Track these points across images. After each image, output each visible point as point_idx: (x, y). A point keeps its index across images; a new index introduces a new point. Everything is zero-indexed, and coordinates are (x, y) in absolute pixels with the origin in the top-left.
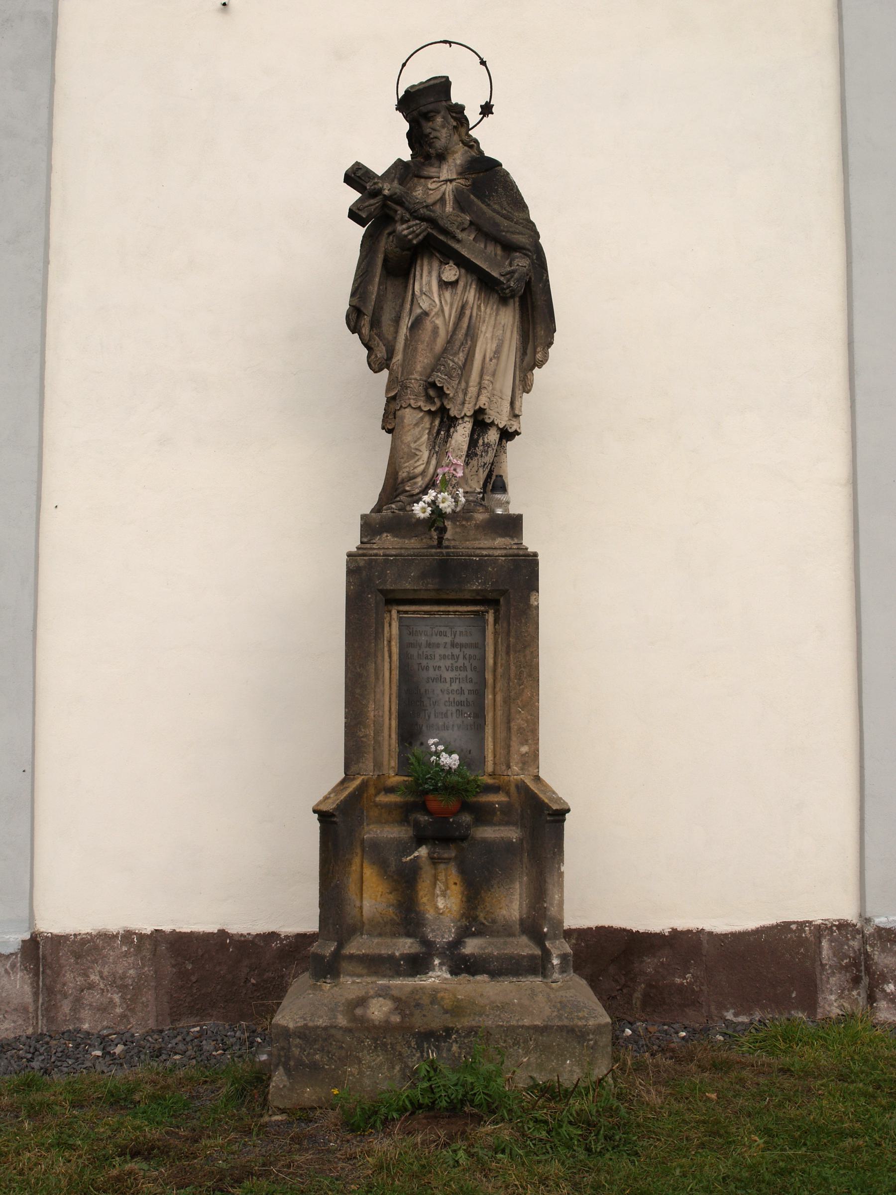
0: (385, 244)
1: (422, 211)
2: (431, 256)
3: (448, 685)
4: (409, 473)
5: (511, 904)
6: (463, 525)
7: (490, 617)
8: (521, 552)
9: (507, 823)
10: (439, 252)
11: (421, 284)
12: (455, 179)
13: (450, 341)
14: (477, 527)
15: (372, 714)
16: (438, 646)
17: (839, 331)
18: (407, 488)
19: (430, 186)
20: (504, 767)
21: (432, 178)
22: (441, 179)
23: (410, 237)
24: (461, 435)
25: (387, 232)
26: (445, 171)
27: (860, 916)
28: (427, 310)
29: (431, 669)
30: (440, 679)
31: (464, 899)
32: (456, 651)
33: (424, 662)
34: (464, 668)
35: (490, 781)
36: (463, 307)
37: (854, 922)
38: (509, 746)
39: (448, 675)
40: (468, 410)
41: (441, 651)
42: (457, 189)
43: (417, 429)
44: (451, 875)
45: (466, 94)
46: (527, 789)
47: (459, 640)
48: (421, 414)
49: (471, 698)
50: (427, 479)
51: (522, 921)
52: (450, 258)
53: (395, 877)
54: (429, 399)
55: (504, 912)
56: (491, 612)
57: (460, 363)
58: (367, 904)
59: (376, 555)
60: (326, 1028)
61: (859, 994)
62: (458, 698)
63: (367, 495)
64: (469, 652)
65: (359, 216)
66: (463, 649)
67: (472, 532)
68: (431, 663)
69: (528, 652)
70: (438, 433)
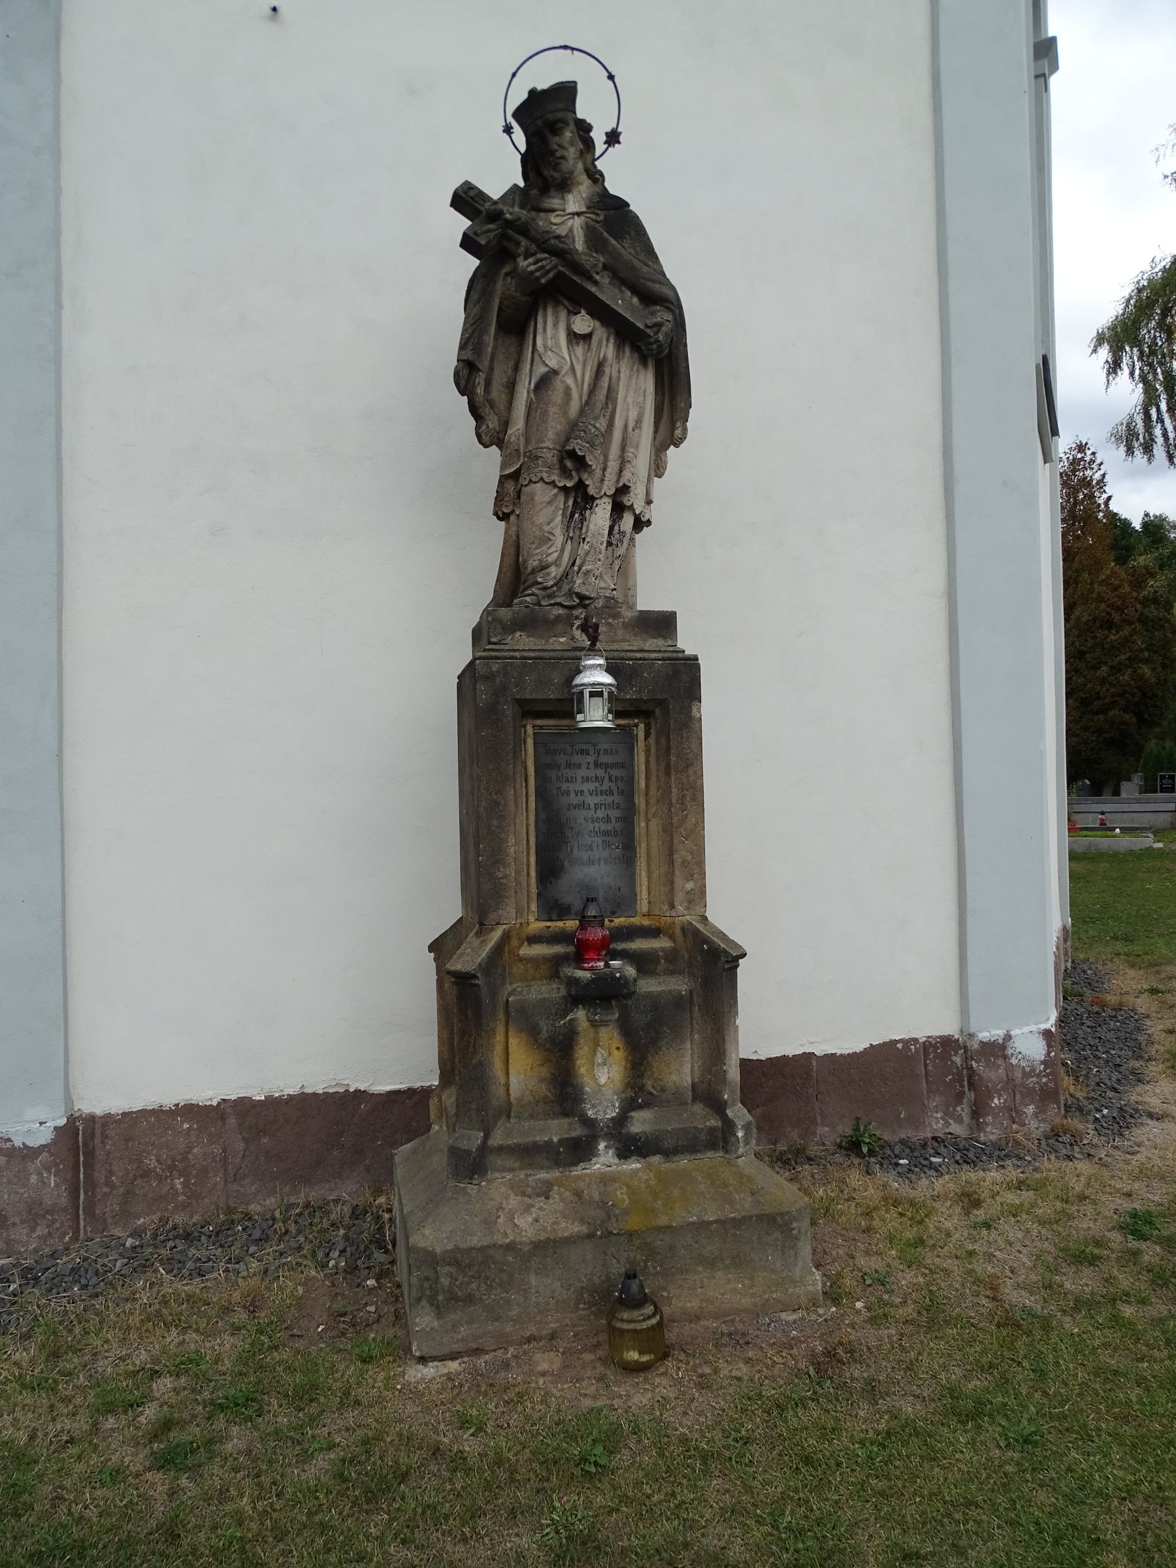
0: (503, 286)
1: (552, 241)
2: (557, 303)
3: (592, 812)
4: (541, 561)
5: (680, 1068)
6: (609, 624)
7: (641, 731)
8: (680, 655)
9: (673, 973)
10: (569, 299)
11: (545, 339)
12: (583, 213)
13: (588, 403)
14: (625, 625)
15: (512, 850)
16: (579, 766)
17: (936, 439)
18: (539, 580)
19: (553, 220)
20: (666, 907)
21: (553, 211)
22: (568, 211)
23: (537, 274)
24: (601, 515)
25: (504, 271)
26: (571, 203)
27: (962, 1031)
28: (556, 368)
29: (573, 795)
30: (583, 806)
31: (629, 1066)
32: (600, 772)
33: (564, 786)
34: (611, 792)
35: (646, 922)
36: (600, 365)
37: (956, 1037)
38: (672, 883)
39: (592, 800)
40: (609, 488)
41: (583, 772)
42: (586, 224)
43: (546, 507)
44: (610, 1037)
45: (592, 108)
46: (697, 932)
47: (608, 759)
48: (556, 491)
49: (618, 826)
50: (561, 570)
51: (694, 1086)
52: (581, 306)
53: (548, 1046)
54: (565, 472)
55: (674, 1077)
56: (642, 726)
57: (603, 430)
58: (514, 1081)
59: (512, 658)
60: (482, 1249)
61: (963, 1110)
62: (604, 827)
63: (481, 589)
64: (615, 772)
65: (476, 242)
66: (609, 770)
67: (620, 632)
68: (572, 787)
69: (691, 771)
70: (572, 516)
